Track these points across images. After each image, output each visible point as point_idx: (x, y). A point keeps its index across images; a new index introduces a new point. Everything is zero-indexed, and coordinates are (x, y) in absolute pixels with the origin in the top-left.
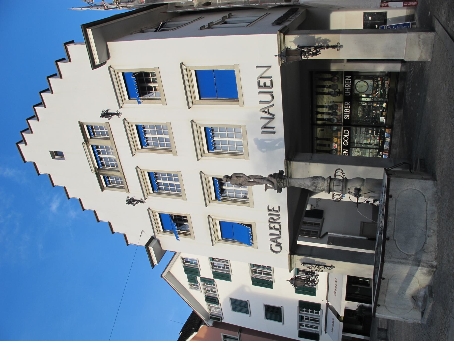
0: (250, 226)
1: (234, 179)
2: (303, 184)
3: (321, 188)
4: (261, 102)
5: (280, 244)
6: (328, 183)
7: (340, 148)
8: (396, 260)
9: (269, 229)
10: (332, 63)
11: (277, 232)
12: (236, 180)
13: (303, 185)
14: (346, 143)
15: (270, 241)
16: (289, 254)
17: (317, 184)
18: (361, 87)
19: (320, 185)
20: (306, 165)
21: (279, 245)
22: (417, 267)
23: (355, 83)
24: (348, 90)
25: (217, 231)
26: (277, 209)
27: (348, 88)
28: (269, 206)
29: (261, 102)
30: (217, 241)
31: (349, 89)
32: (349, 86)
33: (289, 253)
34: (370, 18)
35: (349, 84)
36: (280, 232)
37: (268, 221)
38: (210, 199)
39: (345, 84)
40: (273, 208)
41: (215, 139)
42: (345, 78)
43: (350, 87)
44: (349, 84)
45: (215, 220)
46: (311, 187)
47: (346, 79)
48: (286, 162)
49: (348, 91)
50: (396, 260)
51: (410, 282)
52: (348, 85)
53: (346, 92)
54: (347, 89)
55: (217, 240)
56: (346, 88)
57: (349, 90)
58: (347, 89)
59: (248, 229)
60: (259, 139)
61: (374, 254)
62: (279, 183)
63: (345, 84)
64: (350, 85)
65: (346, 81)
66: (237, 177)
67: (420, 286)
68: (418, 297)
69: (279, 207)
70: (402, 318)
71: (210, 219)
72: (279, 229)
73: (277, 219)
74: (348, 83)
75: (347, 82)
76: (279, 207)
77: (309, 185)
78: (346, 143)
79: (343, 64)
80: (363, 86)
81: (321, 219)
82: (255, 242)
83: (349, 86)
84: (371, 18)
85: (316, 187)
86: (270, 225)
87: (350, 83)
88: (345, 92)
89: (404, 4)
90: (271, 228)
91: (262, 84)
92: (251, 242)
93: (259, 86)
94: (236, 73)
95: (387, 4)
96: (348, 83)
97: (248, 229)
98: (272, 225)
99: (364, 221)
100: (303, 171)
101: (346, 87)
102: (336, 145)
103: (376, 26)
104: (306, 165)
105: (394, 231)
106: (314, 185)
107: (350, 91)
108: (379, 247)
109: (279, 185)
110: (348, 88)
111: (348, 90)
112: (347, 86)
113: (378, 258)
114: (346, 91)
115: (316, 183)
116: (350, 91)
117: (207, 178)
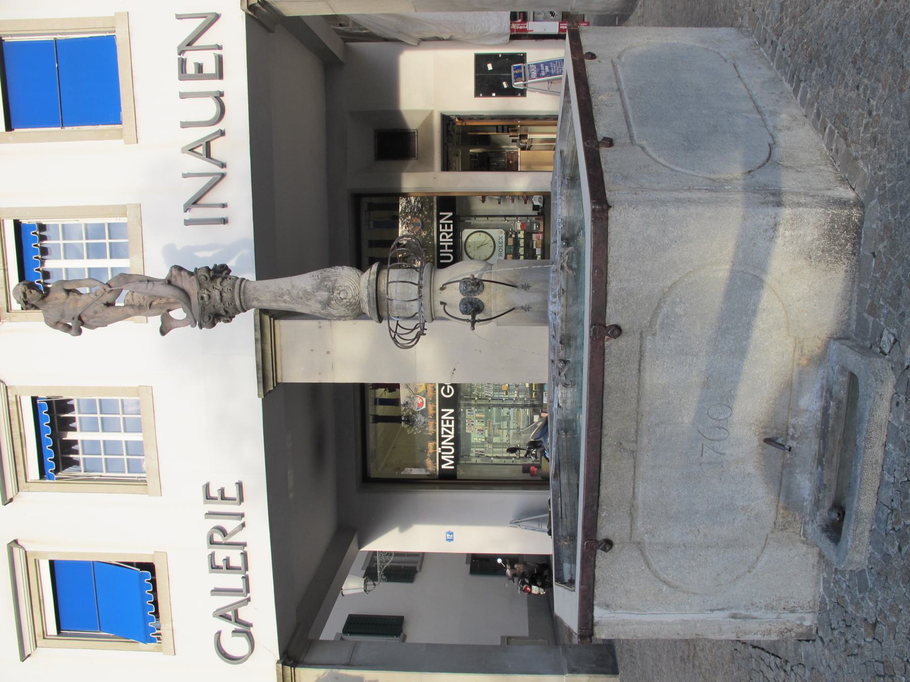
0: (149, 567)
1: (56, 299)
2: (290, 288)
3: (350, 296)
4: (217, 591)
5: (249, 625)
6: (373, 274)
7: (435, 409)
8: (663, 196)
9: (210, 572)
10: (407, 172)
11: (234, 581)
12: (64, 303)
13: (289, 293)
14: (448, 392)
15: (215, 618)
16: (278, 662)
17: (336, 280)
18: (478, 247)
19: (346, 284)
20: (320, 327)
21: (245, 630)
23: (464, 239)
24: (448, 249)
25: (41, 601)
26: (232, 492)
27: (446, 244)
28: (207, 487)
29: (217, 591)
30: (40, 641)
31: (448, 246)
32: (450, 238)
34: (490, 67)
35: (449, 233)
36: (246, 579)
37: (205, 541)
38: (21, 478)
39: (439, 233)
40: (222, 491)
41: (49, 265)
42: (440, 217)
43: (452, 240)
44: (449, 233)
45: (37, 558)
46: (316, 294)
47: (441, 221)
48: (258, 317)
49: (446, 250)
50: (663, 196)
51: (748, 327)
52: (448, 237)
53: (441, 255)
54: (443, 247)
55: (39, 636)
56: (441, 244)
57: (449, 247)
58: (445, 246)
59: (142, 577)
60: (179, 248)
62: (208, 290)
63: (439, 233)
64: (452, 234)
65: (441, 226)
66: (68, 291)
67: (798, 352)
68: (793, 438)
69: (240, 485)
70: (727, 613)
71: (18, 553)
72: (243, 569)
73: (234, 533)
74: (446, 230)
75: (443, 228)
76: (240, 485)
77: (309, 288)
78: (448, 392)
79: (431, 174)
80: (482, 245)
81: (398, 638)
82: (165, 630)
83: (449, 238)
84: (494, 92)
85: (332, 290)
86: (212, 556)
87: (451, 230)
88: (439, 253)
89: (561, 27)
90: (214, 567)
91: (191, 69)
92: (153, 630)
93: (214, 567)
94: (119, 42)
95: (525, 26)
96: (446, 230)
97: (142, 577)
98: (221, 555)
99: (510, 635)
100: (312, 350)
101: (441, 240)
102: (424, 399)
103: (504, 84)
104: (320, 327)
105: (629, 126)
106: (326, 283)
107: (452, 251)
109: (205, 296)
110: (446, 244)
111: (448, 249)
112: (444, 237)
114: (441, 251)
115: (333, 278)
116: (452, 251)
117: (12, 399)
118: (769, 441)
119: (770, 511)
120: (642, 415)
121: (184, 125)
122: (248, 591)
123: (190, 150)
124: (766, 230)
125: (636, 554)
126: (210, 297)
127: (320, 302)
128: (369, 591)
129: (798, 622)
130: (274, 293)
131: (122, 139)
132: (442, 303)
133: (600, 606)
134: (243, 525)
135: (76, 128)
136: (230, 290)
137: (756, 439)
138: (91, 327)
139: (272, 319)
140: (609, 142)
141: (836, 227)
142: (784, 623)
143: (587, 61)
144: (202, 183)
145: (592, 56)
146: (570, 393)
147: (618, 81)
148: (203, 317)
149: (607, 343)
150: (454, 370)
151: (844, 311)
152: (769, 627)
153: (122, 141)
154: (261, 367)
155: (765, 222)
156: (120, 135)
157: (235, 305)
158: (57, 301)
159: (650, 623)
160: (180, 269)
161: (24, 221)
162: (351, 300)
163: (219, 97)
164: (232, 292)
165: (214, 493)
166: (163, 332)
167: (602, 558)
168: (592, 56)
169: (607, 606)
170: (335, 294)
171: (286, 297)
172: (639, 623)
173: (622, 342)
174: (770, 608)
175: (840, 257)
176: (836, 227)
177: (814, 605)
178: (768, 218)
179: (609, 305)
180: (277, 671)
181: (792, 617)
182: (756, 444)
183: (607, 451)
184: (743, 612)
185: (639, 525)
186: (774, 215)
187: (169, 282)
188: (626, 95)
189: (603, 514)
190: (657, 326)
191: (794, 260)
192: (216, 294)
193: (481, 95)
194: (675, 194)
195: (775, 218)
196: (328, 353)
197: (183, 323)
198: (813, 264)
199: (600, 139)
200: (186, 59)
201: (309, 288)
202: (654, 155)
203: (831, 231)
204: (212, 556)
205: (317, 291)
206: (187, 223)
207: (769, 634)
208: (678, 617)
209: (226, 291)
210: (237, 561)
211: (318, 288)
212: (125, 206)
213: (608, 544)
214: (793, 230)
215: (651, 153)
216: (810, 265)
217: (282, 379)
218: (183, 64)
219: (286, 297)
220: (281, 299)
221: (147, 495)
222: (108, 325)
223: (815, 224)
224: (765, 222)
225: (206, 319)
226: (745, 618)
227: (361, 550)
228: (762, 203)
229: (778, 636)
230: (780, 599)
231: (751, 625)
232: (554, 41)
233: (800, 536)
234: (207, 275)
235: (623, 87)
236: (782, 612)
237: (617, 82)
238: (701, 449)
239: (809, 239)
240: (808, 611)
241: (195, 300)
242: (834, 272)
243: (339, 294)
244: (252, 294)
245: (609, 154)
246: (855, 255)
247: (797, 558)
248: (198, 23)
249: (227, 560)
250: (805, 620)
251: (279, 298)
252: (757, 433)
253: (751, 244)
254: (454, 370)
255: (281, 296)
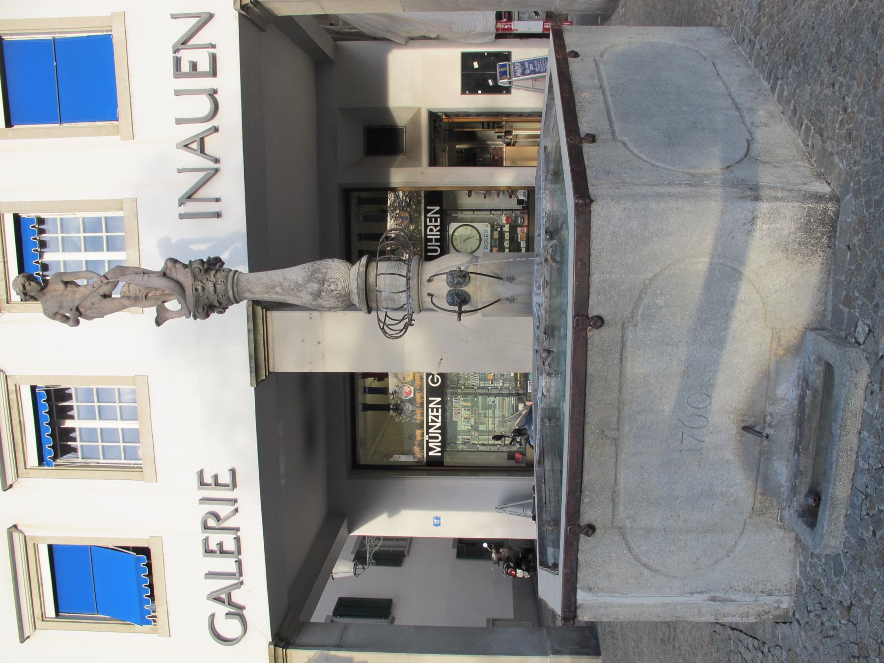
0: (145, 551)
1: (55, 290)
2: (281, 280)
3: (340, 288)
4: (211, 575)
5: (242, 608)
6: (363, 266)
7: (422, 398)
8: (644, 190)
9: (204, 556)
10: (395, 167)
11: (228, 565)
12: (62, 295)
13: (281, 285)
14: (436, 381)
15: (209, 601)
16: (270, 644)
17: (326, 272)
18: (465, 240)
19: (336, 276)
20: (311, 318)
21: (238, 612)
22: (749, 205)
23: (451, 232)
24: (436, 242)
25: (40, 585)
26: (225, 478)
27: (433, 237)
28: (201, 474)
29: (211, 575)
30: (39, 623)
31: (435, 239)
32: (437, 231)
33: (271, 640)
34: (476, 65)
35: (436, 227)
36: (239, 562)
37: (199, 526)
38: (21, 465)
39: (426, 226)
40: (216, 477)
41: (48, 257)
42: (427, 211)
43: (439, 233)
44: (436, 227)
45: (36, 542)
46: (307, 286)
47: (429, 215)
48: (251, 308)
49: (433, 243)
50: (644, 190)
51: (727, 318)
52: (435, 230)
53: (429, 248)
54: (431, 240)
55: (38, 619)
56: (428, 237)
57: (436, 240)
58: (432, 239)
59: (138, 561)
60: (174, 241)
61: (532, 542)
62: (202, 282)
63: (426, 226)
64: (439, 228)
65: (428, 219)
66: (66, 283)
67: (775, 343)
68: (770, 425)
69: (233, 472)
70: (706, 596)
72: (236, 553)
73: (227, 518)
74: (433, 223)
75: (431, 221)
76: (233, 472)
77: (300, 280)
78: (436, 381)
79: (418, 169)
80: (468, 239)
81: (387, 621)
82: (160, 613)
83: (437, 232)
84: (480, 90)
85: (322, 282)
86: (206, 541)
87: (438, 224)
88: (426, 246)
89: (545, 27)
90: (208, 552)
91: (185, 67)
92: (148, 612)
93: (208, 552)
94: (115, 41)
95: (510, 25)
96: (433, 223)
97: (138, 561)
98: (215, 539)
99: (495, 617)
100: (303, 341)
101: (429, 233)
102: (412, 388)
103: (490, 81)
104: (311, 318)
105: (611, 123)
106: (317, 275)
107: (439, 244)
108: (546, 460)
109: (199, 288)
110: (433, 237)
111: (436, 242)
112: (431, 230)
113: (547, 493)
114: (429, 244)
115: (323, 271)
116: (439, 244)
117: (12, 388)
118: (747, 429)
119: (748, 496)
120: (624, 404)
121: (179, 121)
122: (241, 574)
123: (184, 146)
124: (744, 223)
125: (618, 538)
126: (204, 288)
127: (311, 294)
128: (359, 574)
129: (776, 605)
130: (266, 285)
131: (118, 135)
132: (429, 295)
133: (582, 589)
134: (236, 510)
135: (73, 124)
136: (223, 282)
137: (734, 427)
138: (89, 318)
139: (264, 310)
140: (592, 138)
141: (812, 220)
142: (762, 606)
143: (570, 60)
144: (196, 177)
145: (576, 55)
146: (553, 382)
147: (600, 79)
148: (197, 308)
149: (589, 334)
150: (441, 359)
151: (820, 303)
152: (747, 610)
153: (119, 137)
154: (253, 357)
155: (743, 215)
156: (117, 132)
157: (228, 297)
158: (56, 293)
159: (631, 606)
160: (175, 261)
161: (23, 215)
162: (341, 292)
163: (212, 94)
164: (226, 284)
165: (208, 479)
166: (159, 322)
167: (585, 543)
168: (576, 55)
169: (590, 589)
170: (325, 286)
171: (278, 289)
172: (621, 606)
173: (604, 332)
174: (748, 591)
175: (816, 250)
176: (812, 220)
177: (791, 588)
178: (746, 212)
179: (592, 296)
180: (269, 652)
181: (769, 600)
182: (734, 431)
183: (589, 438)
184: (721, 595)
185: (621, 510)
186: (751, 209)
187: (164, 274)
188: (608, 92)
189: (586, 500)
190: (639, 317)
191: (771, 252)
192: (210, 286)
193: (467, 92)
194: (656, 189)
195: (753, 212)
196: (319, 343)
197: (178, 314)
198: (790, 256)
199: (582, 136)
200: (181, 57)
201: (300, 280)
202: (635, 151)
203: (807, 224)
204: (206, 541)
205: (308, 283)
206: (182, 216)
207: (747, 616)
208: (659, 600)
209: (219, 283)
210: (230, 545)
211: (309, 280)
212: (121, 200)
213: (591, 529)
214: (771, 224)
215: (632, 149)
216: (787, 258)
217: (274, 368)
218: (177, 62)
219: (278, 289)
220: (273, 291)
221: (143, 482)
222: (105, 316)
223: (792, 218)
224: (743, 215)
225: (200, 310)
226: (724, 600)
227: (351, 534)
228: (740, 198)
229: (756, 618)
230: (758, 582)
231: (729, 608)
232: (538, 40)
233: (777, 521)
234: (201, 267)
235: (605, 84)
236: (760, 595)
237: (599, 80)
238: (681, 437)
239: (786, 232)
240: (785, 594)
241: (189, 291)
242: (810, 264)
243: (329, 286)
244: (245, 286)
245: (591, 150)
246: (830, 247)
247: (774, 543)
248: (192, 22)
249: (221, 545)
250: (782, 602)
251: (271, 290)
252: (735, 421)
253: (730, 238)
254: (441, 359)
255: (273, 287)
